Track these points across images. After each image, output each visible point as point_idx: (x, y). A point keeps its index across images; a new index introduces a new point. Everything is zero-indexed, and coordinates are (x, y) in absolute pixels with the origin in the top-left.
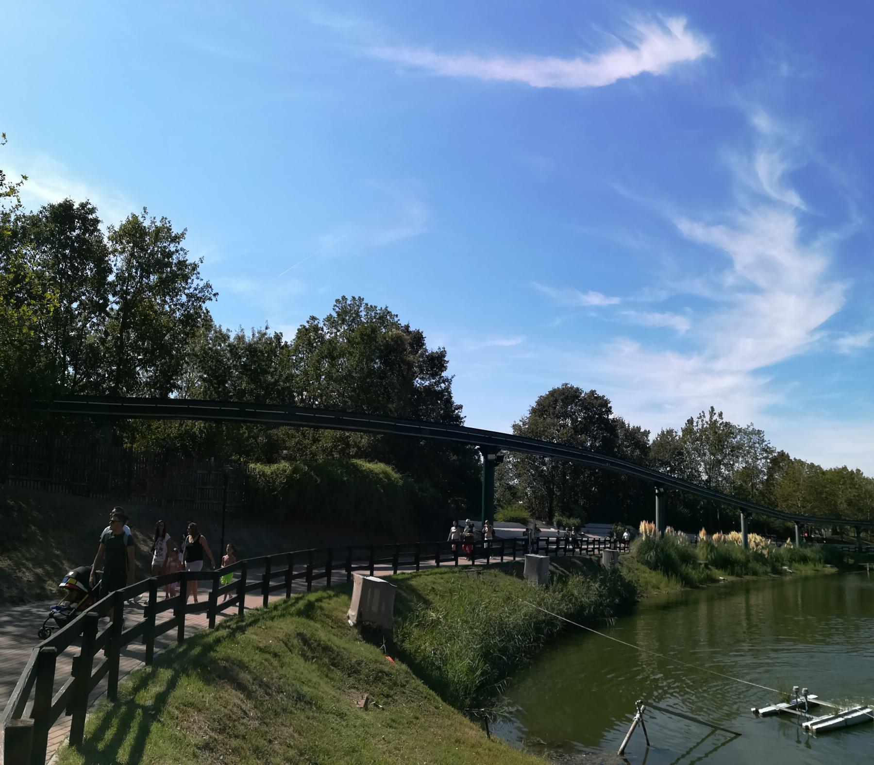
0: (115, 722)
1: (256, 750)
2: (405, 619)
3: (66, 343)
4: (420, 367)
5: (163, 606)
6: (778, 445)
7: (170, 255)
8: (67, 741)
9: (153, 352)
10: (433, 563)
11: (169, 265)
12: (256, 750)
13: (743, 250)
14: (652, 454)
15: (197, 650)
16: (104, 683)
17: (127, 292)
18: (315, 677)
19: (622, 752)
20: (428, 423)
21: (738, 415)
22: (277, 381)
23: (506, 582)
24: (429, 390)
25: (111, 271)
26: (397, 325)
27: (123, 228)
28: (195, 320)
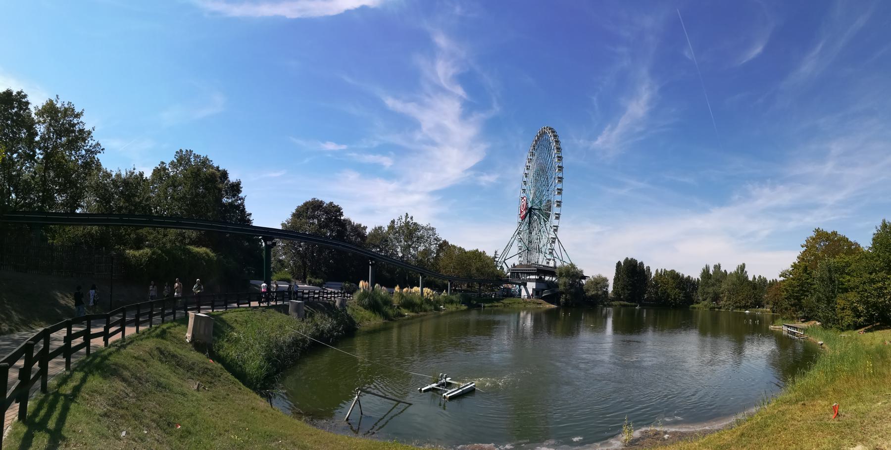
0: (46, 405)
1: (135, 416)
2: (219, 337)
3: (10, 179)
4: (226, 191)
5: (77, 335)
6: (443, 236)
7: (74, 125)
8: (17, 418)
9: (65, 185)
10: (236, 305)
11: (74, 131)
12: (135, 416)
13: (427, 119)
14: (368, 241)
15: (98, 360)
16: (38, 383)
17: (47, 148)
18: (167, 373)
19: (347, 419)
20: (231, 224)
21: (421, 219)
22: (141, 201)
23: (279, 316)
24: (231, 204)
25: (37, 134)
26: (212, 167)
27: (44, 108)
28: (91, 165)
